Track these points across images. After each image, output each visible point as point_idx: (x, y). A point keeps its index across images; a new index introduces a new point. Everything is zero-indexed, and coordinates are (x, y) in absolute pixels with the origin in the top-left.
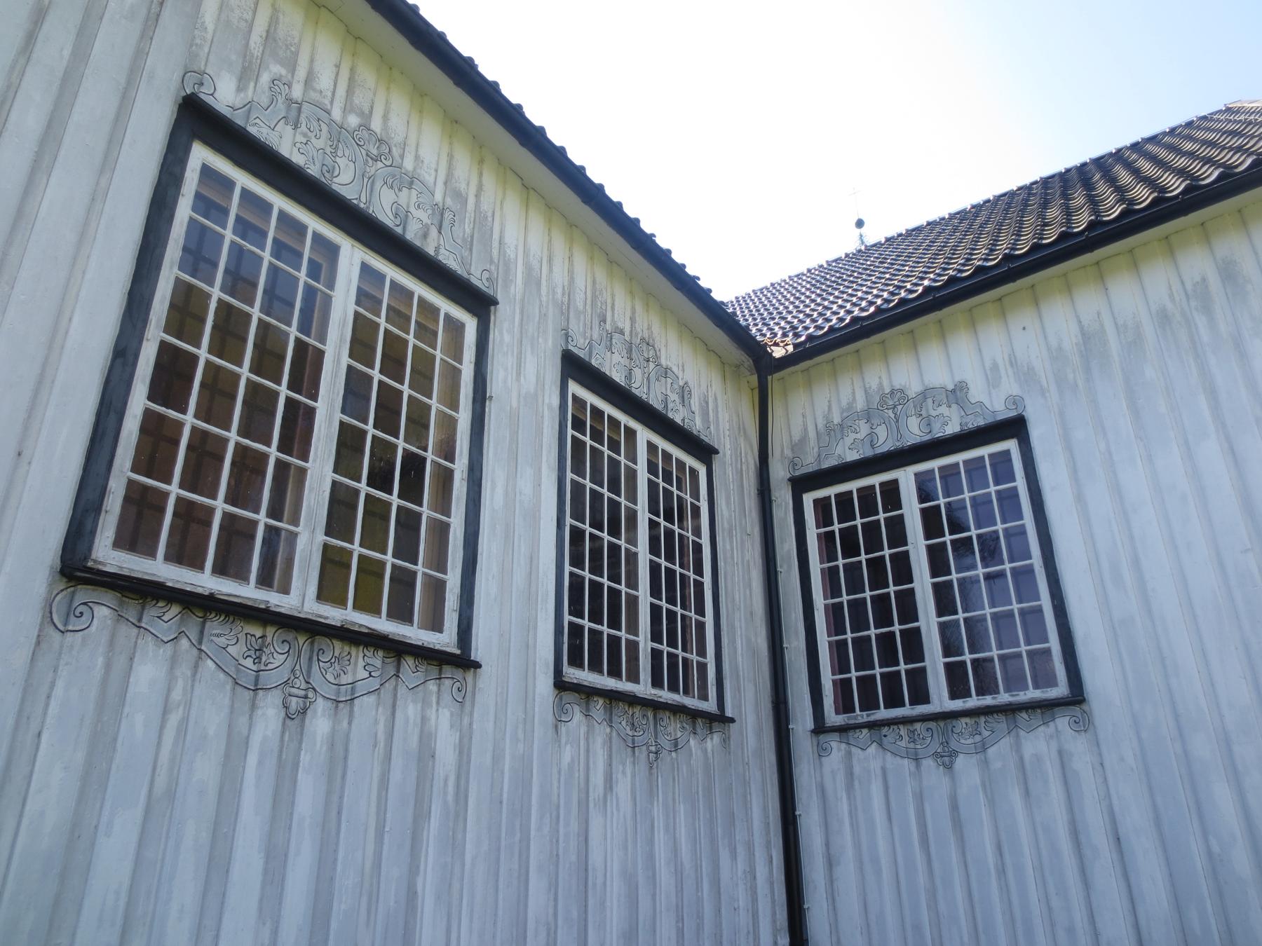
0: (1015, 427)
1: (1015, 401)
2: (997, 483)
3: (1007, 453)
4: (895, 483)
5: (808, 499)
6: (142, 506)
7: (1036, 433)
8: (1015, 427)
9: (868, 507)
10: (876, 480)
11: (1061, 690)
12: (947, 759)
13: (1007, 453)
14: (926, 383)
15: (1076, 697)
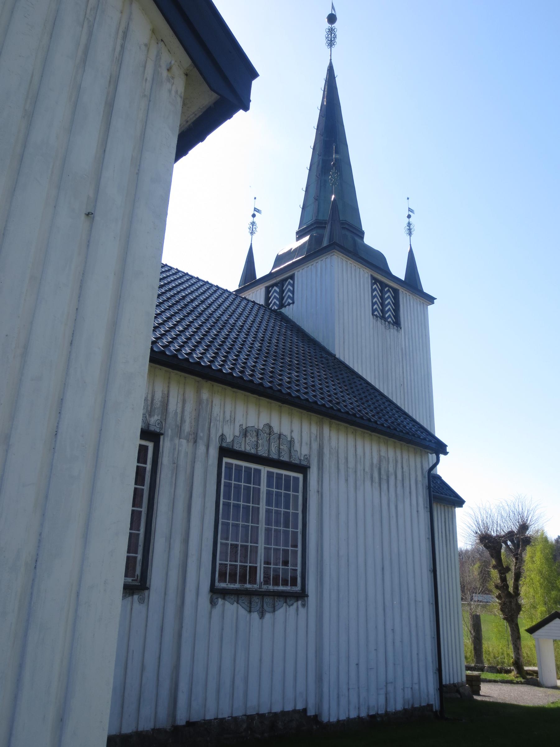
0: (303, 469)
11: (298, 588)
15: (302, 596)
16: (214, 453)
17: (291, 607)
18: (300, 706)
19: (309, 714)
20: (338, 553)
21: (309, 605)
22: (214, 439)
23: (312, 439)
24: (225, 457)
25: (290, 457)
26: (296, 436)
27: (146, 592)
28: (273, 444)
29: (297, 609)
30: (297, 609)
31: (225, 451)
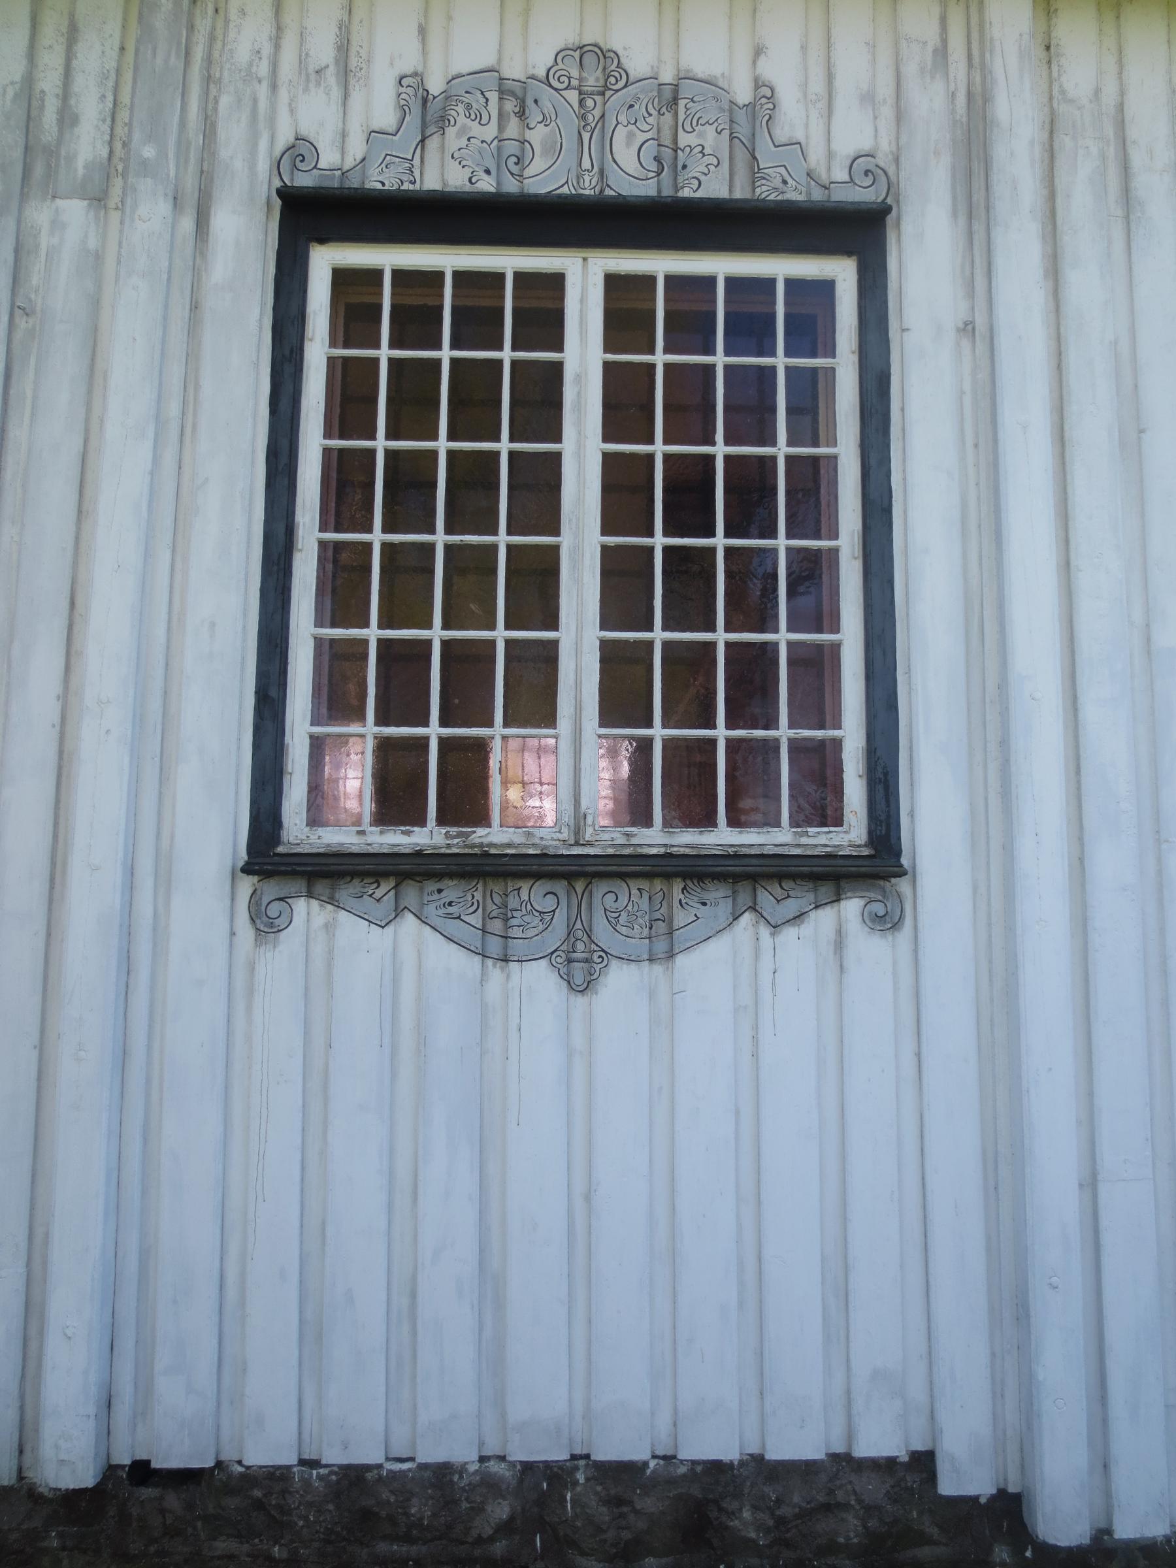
0: (857, 228)
1: (864, 165)
2: (444, 723)
3: (826, 288)
4: (556, 281)
5: (324, 261)
6: (811, 331)
7: (215, 827)
8: (857, 228)
9: (750, 329)
10: (508, 261)
11: (851, 833)
12: (580, 969)
13: (826, 288)
14: (684, 64)
15: (878, 866)
16: (243, 235)
17: (790, 934)
18: (879, 1440)
19: (947, 1487)
20: (1148, 640)
21: (924, 919)
22: (238, 164)
23: (910, 70)
24: (322, 241)
25: (755, 173)
26: (782, 70)
27: (903, 885)
28: (621, 134)
29: (839, 943)
30: (839, 943)
31: (312, 212)
